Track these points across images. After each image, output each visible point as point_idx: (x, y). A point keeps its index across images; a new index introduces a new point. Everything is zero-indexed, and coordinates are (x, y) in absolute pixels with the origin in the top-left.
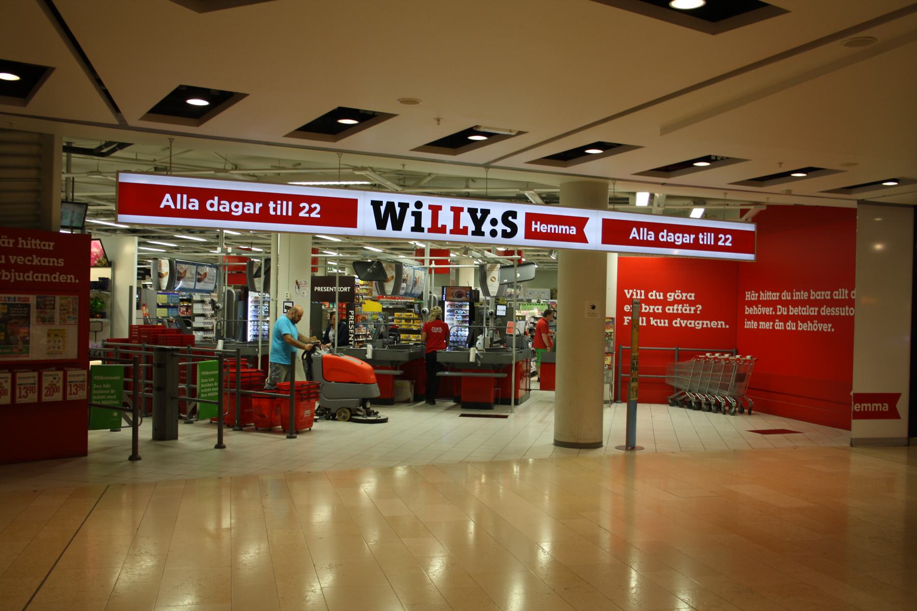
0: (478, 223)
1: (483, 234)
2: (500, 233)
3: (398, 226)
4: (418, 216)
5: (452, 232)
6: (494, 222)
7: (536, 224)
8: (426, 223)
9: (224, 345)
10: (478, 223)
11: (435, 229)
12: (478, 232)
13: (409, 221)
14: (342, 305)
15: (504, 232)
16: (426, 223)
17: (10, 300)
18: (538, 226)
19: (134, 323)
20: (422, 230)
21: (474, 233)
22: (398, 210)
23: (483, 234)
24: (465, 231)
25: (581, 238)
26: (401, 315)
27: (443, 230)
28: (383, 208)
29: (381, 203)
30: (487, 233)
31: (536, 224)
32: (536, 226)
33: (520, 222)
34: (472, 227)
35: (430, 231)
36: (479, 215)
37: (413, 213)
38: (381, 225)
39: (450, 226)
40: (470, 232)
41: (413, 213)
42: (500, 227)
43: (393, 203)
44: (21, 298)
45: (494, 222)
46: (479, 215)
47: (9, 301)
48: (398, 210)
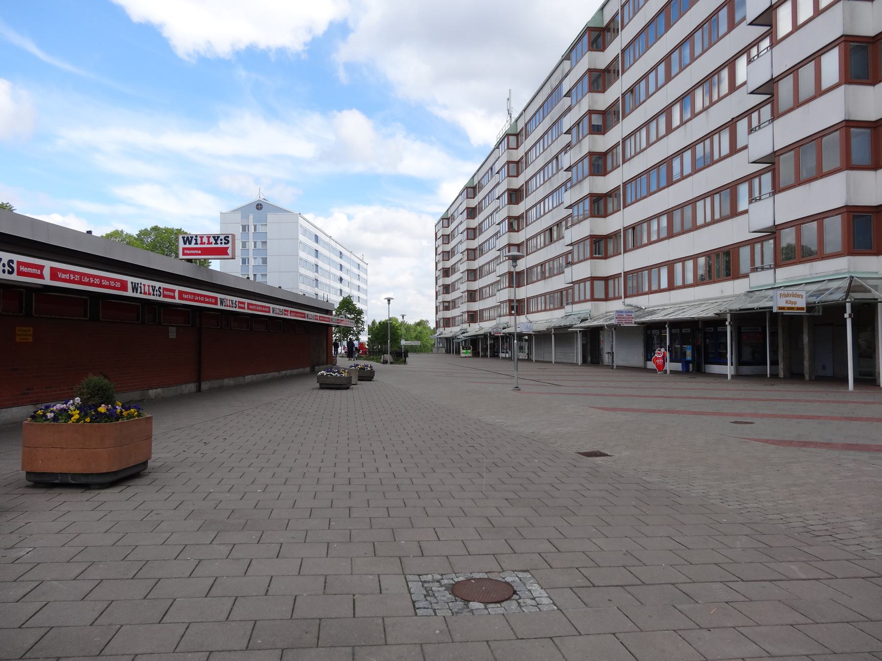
0: (216, 241)
1: (218, 244)
2: (223, 243)
3: (190, 243)
4: (196, 240)
5: (207, 244)
6: (221, 240)
7: (22, 267)
8: (199, 241)
9: (659, 325)
10: (216, 241)
11: (202, 243)
12: (216, 243)
13: (194, 241)
14: (108, 407)
15: (225, 242)
16: (199, 241)
17: (219, 242)
18: (23, 269)
19: (471, 356)
20: (198, 244)
21: (215, 244)
22: (190, 239)
23: (218, 244)
24: (211, 243)
25: (41, 276)
26: (563, 71)
27: (204, 243)
28: (185, 239)
29: (185, 237)
30: (219, 244)
31: (22, 267)
32: (22, 269)
33: (15, 266)
34: (214, 242)
35: (200, 244)
36: (216, 238)
37: (195, 239)
38: (185, 243)
39: (207, 242)
40: (213, 243)
41: (195, 239)
42: (223, 241)
44: (252, 305)
45: (221, 240)
46: (216, 238)
47: (216, 243)
48: (190, 239)
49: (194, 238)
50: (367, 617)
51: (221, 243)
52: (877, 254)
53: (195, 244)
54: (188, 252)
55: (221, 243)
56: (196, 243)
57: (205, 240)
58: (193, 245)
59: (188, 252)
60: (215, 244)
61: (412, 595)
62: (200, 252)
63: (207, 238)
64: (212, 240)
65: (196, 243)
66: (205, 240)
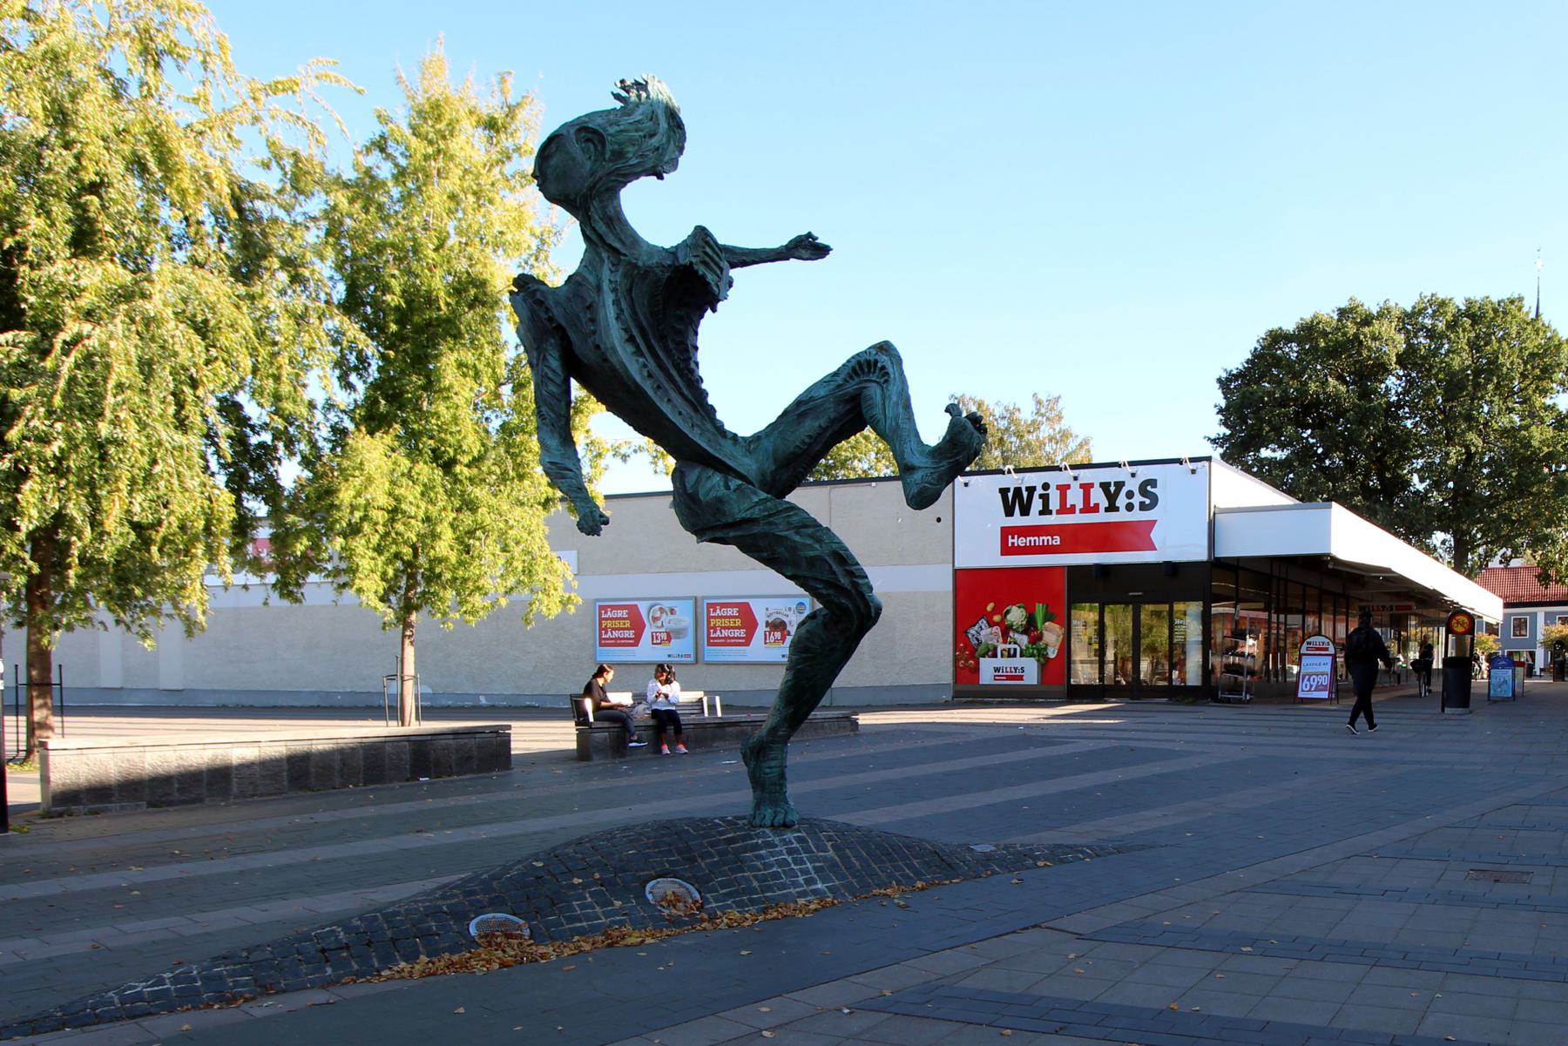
0: (1112, 498)
3: (1025, 511)
5: (1082, 511)
6: (1130, 495)
8: (1054, 504)
10: (1112, 498)
13: (1037, 504)
17: (1121, 501)
20: (1050, 513)
21: (1107, 510)
24: (1096, 509)
28: (1010, 495)
34: (1104, 503)
35: (1058, 512)
36: (1112, 489)
37: (1041, 496)
39: (1080, 505)
40: (1102, 509)
41: (1041, 496)
42: (1138, 499)
43: (1020, 488)
45: (1130, 495)
46: (1112, 489)
48: (1025, 494)
49: (1039, 491)
51: (1130, 507)
53: (1041, 513)
54: (1021, 542)
55: (1130, 507)
56: (1045, 511)
57: (1075, 497)
59: (1021, 542)
62: (1057, 540)
64: (1098, 496)
65: (1045, 511)
66: (1075, 497)
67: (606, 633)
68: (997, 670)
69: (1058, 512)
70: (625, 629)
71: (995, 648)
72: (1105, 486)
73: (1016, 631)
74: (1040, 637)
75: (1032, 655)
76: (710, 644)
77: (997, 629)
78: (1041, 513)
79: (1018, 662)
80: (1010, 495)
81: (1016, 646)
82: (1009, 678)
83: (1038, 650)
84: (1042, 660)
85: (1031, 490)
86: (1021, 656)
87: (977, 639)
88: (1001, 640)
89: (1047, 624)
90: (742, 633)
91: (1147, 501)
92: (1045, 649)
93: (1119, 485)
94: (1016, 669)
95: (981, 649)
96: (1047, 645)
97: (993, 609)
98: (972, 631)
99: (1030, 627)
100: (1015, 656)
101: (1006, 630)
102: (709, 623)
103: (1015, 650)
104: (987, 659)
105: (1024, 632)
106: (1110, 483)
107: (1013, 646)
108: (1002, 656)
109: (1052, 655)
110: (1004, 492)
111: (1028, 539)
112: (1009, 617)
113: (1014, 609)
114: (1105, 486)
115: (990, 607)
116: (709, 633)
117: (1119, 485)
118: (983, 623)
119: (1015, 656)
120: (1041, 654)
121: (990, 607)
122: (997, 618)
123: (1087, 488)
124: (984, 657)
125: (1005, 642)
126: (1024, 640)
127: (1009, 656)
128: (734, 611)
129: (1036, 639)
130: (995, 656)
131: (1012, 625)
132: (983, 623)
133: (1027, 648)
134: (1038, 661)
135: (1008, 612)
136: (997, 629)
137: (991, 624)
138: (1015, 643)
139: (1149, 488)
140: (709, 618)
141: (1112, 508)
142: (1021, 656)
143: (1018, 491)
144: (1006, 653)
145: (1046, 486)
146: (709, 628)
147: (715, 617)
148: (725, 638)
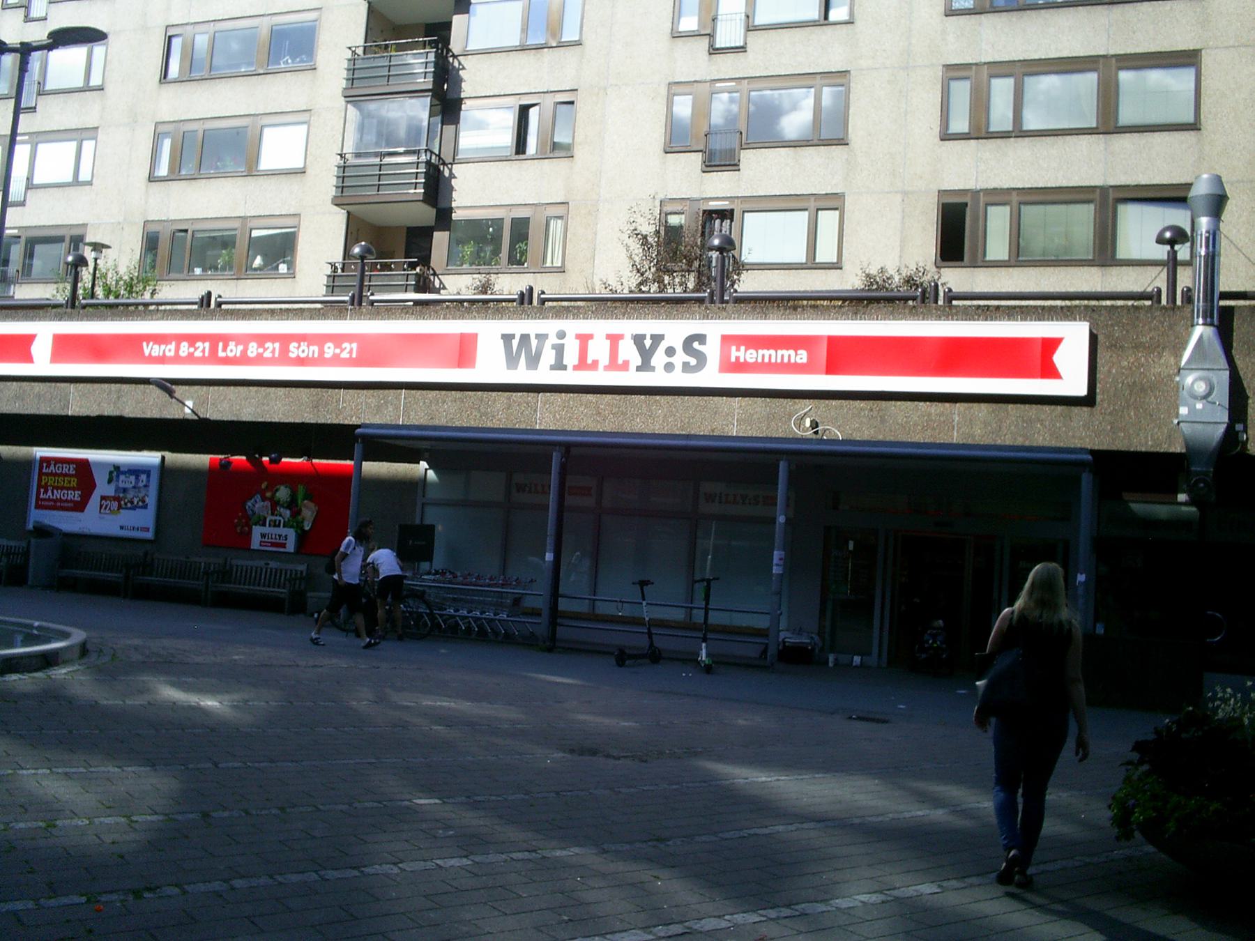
0: (646, 356)
2: (678, 367)
3: (533, 362)
5: (607, 368)
6: (670, 351)
8: (571, 358)
10: (646, 356)
13: (548, 357)
16: (571, 358)
17: (659, 359)
20: (564, 368)
21: (638, 369)
24: (625, 366)
28: (515, 343)
34: (636, 360)
35: (576, 368)
36: (648, 343)
37: (554, 347)
39: (604, 360)
40: (633, 367)
41: (554, 347)
42: (680, 357)
45: (670, 351)
46: (648, 343)
48: (534, 342)
50: (715, 917)
51: (669, 367)
52: (2, 414)
53: (553, 368)
54: (751, 356)
55: (669, 367)
56: (559, 366)
57: (274, 536)
58: (266, 540)
59: (751, 356)
60: (638, 369)
61: (23, 117)
62: (802, 356)
63: (578, 342)
65: (559, 366)
66: (274, 536)
67: (46, 492)
68: (263, 536)
69: (576, 368)
70: (68, 489)
71: (265, 519)
72: (638, 340)
73: (282, 506)
74: (299, 512)
75: (292, 527)
76: (38, 507)
77: (267, 503)
78: (553, 368)
79: (282, 531)
80: (515, 343)
81: (281, 518)
82: (273, 545)
83: (297, 523)
84: (299, 531)
85: (542, 337)
86: (284, 526)
87: (253, 511)
88: (270, 512)
89: (306, 502)
90: (75, 496)
91: (693, 362)
92: (302, 522)
93: (657, 339)
94: (280, 536)
95: (255, 519)
96: (303, 519)
97: (267, 487)
98: (249, 504)
99: (292, 504)
100: (279, 526)
101: (275, 504)
102: (40, 480)
103: (280, 521)
104: (258, 527)
105: (288, 508)
106: (645, 335)
107: (278, 518)
108: (270, 525)
109: (307, 528)
110: (507, 338)
111: (761, 352)
112: (277, 494)
113: (282, 488)
114: (638, 340)
115: (263, 486)
116: (38, 493)
117: (657, 339)
118: (258, 497)
119: (279, 526)
120: (299, 527)
121: (263, 486)
122: (268, 494)
123: (614, 339)
124: (256, 525)
125: (273, 514)
126: (288, 513)
127: (275, 526)
128: (72, 470)
129: (296, 513)
130: (264, 525)
131: (279, 501)
132: (258, 497)
133: (289, 520)
134: (296, 532)
135: (277, 490)
136: (267, 503)
137: (264, 499)
138: (281, 515)
139: (696, 345)
140: (41, 474)
141: (645, 366)
142: (284, 526)
143: (525, 338)
144: (272, 524)
145: (562, 335)
146: (39, 486)
147: (47, 474)
148: (55, 501)
